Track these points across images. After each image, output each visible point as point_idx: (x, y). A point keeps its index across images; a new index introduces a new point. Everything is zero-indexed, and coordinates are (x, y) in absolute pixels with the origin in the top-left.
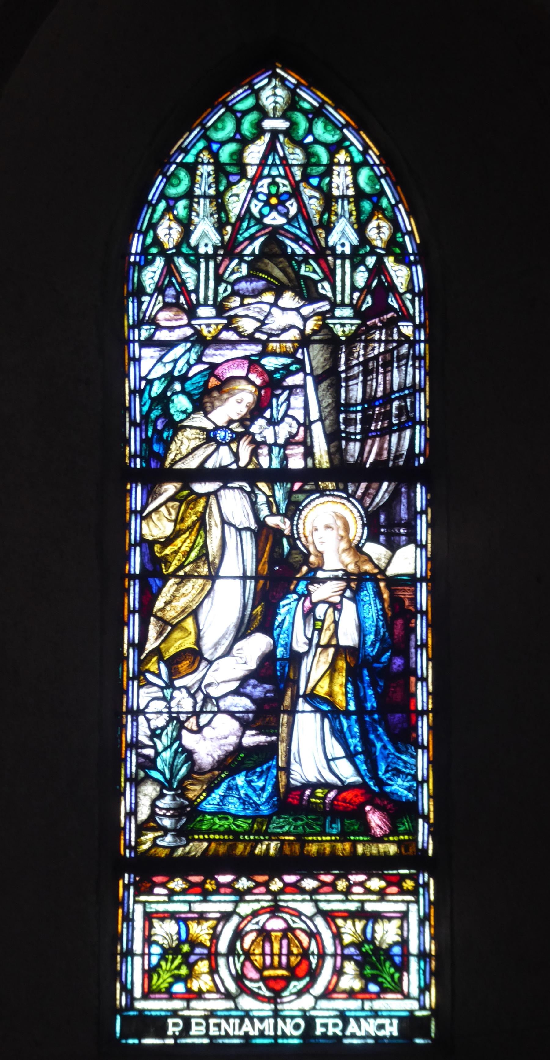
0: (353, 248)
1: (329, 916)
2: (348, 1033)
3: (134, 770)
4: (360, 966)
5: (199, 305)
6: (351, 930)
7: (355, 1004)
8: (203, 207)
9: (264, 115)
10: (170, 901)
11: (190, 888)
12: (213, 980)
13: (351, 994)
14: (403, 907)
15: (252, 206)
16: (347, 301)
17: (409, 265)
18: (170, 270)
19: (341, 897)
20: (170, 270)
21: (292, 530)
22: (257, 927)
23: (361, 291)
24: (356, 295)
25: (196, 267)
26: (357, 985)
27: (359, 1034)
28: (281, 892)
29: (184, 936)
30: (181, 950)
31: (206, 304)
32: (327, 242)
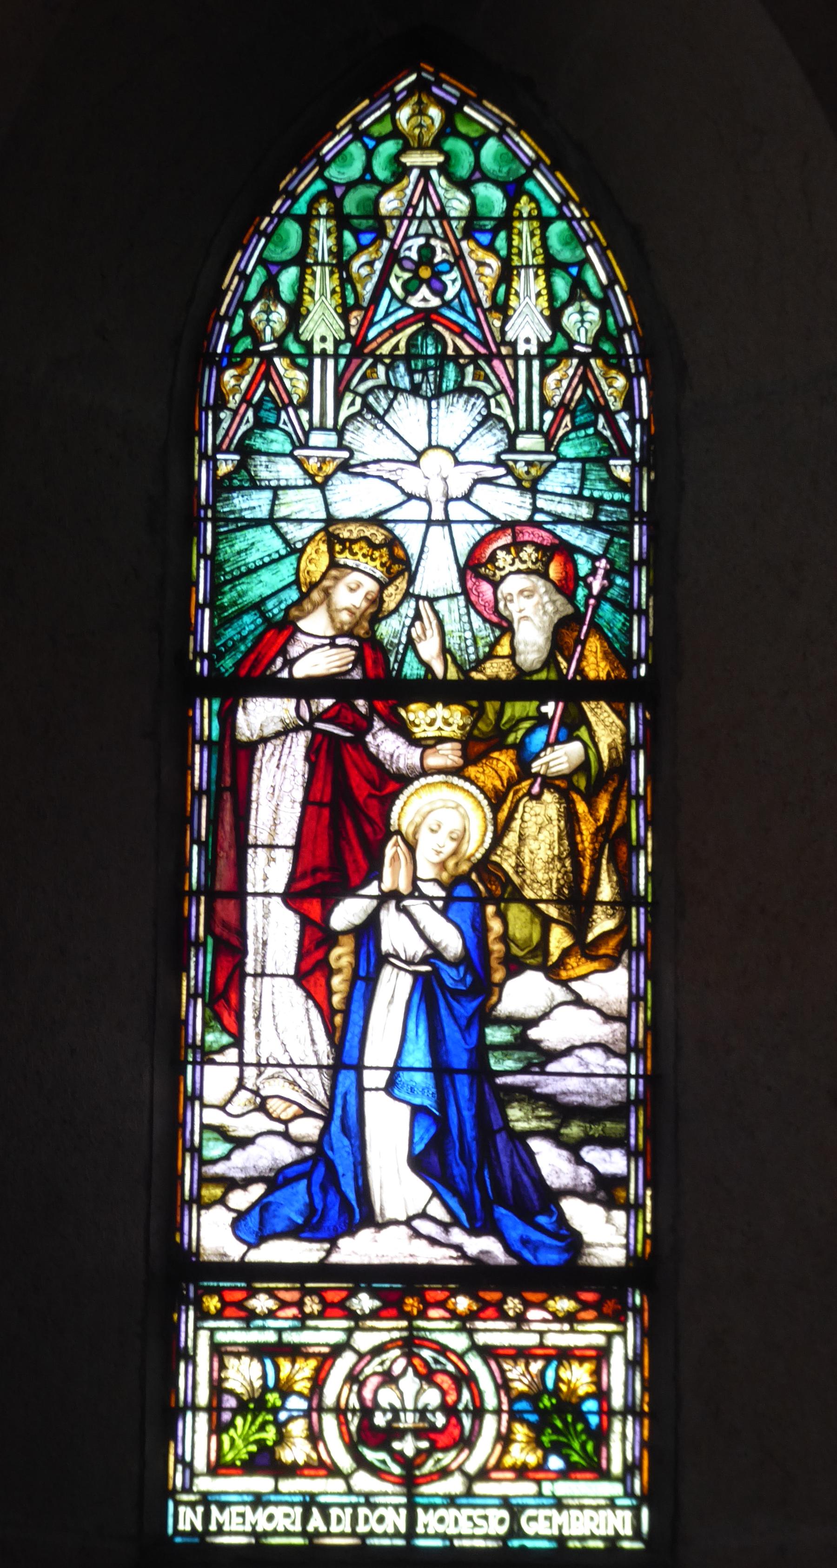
1: (488, 1353)
4: (537, 1429)
6: (519, 1376)
7: (528, 1488)
8: (323, 282)
10: (303, 1328)
11: (481, 1310)
13: (522, 1472)
14: (601, 1340)
17: (625, 370)
19: (512, 1325)
21: (468, 779)
22: (379, 1369)
25: (308, 371)
26: (533, 1459)
29: (271, 1383)
30: (266, 1402)
32: (503, 333)
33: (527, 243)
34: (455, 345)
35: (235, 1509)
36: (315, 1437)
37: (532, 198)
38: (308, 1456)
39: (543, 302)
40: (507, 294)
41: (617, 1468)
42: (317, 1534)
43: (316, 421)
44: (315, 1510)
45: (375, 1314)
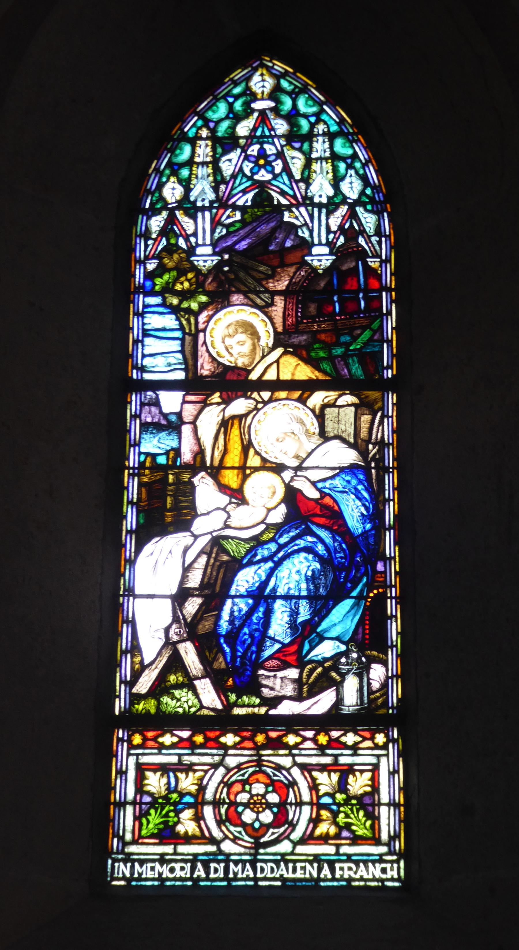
0: (329, 198)
2: (322, 876)
3: (142, 281)
5: (198, 245)
7: (330, 849)
9: (254, 97)
10: (160, 753)
12: (200, 827)
14: (374, 760)
15: (244, 166)
16: (324, 241)
18: (172, 220)
20: (172, 220)
23: (335, 233)
24: (331, 236)
27: (366, 876)
28: (264, 747)
31: (204, 245)
33: (320, 147)
34: (278, 200)
35: (149, 865)
36: (198, 818)
37: (325, 123)
38: (194, 829)
39: (330, 176)
40: (310, 172)
41: (384, 837)
42: (199, 879)
43: (200, 242)
44: (199, 865)
45: (235, 746)
